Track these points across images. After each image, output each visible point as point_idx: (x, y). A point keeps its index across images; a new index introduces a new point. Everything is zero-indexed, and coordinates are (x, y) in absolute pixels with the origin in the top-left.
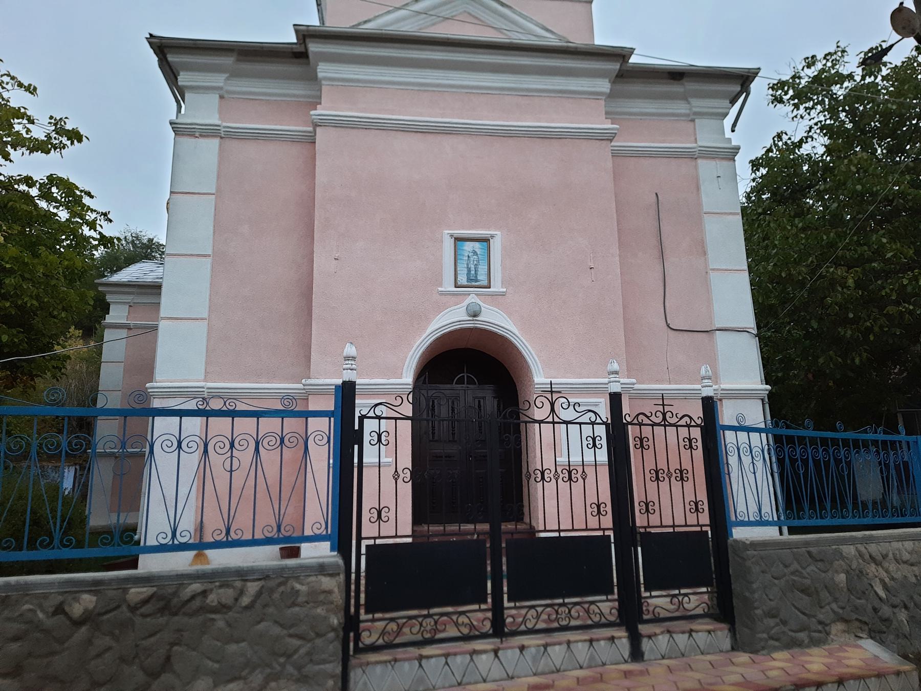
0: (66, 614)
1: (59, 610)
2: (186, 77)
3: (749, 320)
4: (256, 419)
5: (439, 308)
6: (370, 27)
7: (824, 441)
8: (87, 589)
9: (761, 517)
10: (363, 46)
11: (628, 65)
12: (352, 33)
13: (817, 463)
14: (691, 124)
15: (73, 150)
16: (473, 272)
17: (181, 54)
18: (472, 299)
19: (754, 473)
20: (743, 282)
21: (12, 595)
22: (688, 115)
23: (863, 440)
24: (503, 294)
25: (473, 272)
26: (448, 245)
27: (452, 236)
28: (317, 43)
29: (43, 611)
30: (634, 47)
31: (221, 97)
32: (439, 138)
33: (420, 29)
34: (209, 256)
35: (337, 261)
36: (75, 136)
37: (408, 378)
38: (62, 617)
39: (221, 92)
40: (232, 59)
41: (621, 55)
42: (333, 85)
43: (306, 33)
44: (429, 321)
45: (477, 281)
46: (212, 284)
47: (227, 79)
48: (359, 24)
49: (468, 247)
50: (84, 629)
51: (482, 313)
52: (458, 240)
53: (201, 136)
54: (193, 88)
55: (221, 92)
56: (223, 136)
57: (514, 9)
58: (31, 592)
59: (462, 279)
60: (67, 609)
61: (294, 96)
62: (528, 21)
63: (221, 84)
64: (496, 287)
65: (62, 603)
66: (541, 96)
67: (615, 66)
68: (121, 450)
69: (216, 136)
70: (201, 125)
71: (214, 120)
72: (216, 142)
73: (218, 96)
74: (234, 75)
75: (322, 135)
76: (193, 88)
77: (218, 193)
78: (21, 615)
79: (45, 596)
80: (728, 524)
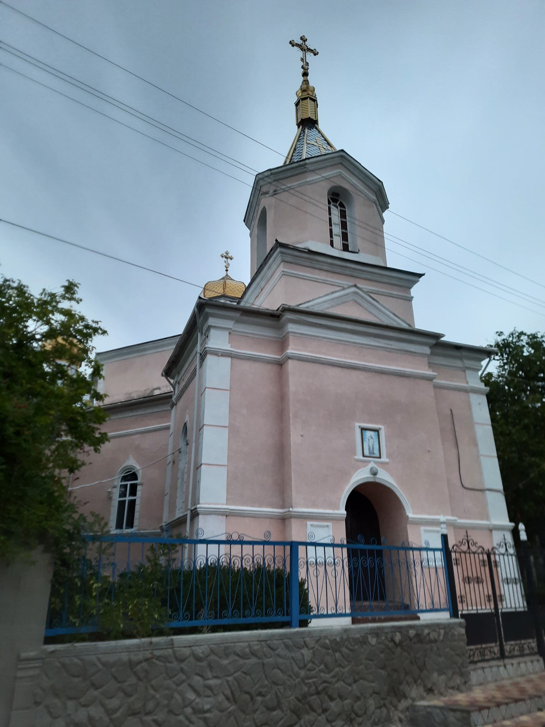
1: (392, 640)
3: (500, 486)
5: (356, 468)
7: (371, 552)
11: (439, 341)
13: (365, 569)
14: (463, 373)
18: (372, 465)
19: (317, 577)
20: (495, 462)
22: (462, 368)
23: (377, 551)
24: (387, 463)
26: (358, 432)
30: (444, 334)
31: (230, 333)
34: (227, 427)
35: (302, 437)
37: (343, 512)
39: (231, 331)
41: (437, 336)
45: (374, 454)
47: (234, 324)
49: (368, 434)
51: (378, 474)
52: (363, 429)
53: (222, 355)
54: (215, 327)
55: (231, 331)
64: (384, 459)
67: (433, 341)
70: (223, 350)
72: (229, 360)
74: (238, 321)
75: (291, 365)
76: (215, 327)
77: (231, 390)
79: (387, 633)
80: (451, 611)
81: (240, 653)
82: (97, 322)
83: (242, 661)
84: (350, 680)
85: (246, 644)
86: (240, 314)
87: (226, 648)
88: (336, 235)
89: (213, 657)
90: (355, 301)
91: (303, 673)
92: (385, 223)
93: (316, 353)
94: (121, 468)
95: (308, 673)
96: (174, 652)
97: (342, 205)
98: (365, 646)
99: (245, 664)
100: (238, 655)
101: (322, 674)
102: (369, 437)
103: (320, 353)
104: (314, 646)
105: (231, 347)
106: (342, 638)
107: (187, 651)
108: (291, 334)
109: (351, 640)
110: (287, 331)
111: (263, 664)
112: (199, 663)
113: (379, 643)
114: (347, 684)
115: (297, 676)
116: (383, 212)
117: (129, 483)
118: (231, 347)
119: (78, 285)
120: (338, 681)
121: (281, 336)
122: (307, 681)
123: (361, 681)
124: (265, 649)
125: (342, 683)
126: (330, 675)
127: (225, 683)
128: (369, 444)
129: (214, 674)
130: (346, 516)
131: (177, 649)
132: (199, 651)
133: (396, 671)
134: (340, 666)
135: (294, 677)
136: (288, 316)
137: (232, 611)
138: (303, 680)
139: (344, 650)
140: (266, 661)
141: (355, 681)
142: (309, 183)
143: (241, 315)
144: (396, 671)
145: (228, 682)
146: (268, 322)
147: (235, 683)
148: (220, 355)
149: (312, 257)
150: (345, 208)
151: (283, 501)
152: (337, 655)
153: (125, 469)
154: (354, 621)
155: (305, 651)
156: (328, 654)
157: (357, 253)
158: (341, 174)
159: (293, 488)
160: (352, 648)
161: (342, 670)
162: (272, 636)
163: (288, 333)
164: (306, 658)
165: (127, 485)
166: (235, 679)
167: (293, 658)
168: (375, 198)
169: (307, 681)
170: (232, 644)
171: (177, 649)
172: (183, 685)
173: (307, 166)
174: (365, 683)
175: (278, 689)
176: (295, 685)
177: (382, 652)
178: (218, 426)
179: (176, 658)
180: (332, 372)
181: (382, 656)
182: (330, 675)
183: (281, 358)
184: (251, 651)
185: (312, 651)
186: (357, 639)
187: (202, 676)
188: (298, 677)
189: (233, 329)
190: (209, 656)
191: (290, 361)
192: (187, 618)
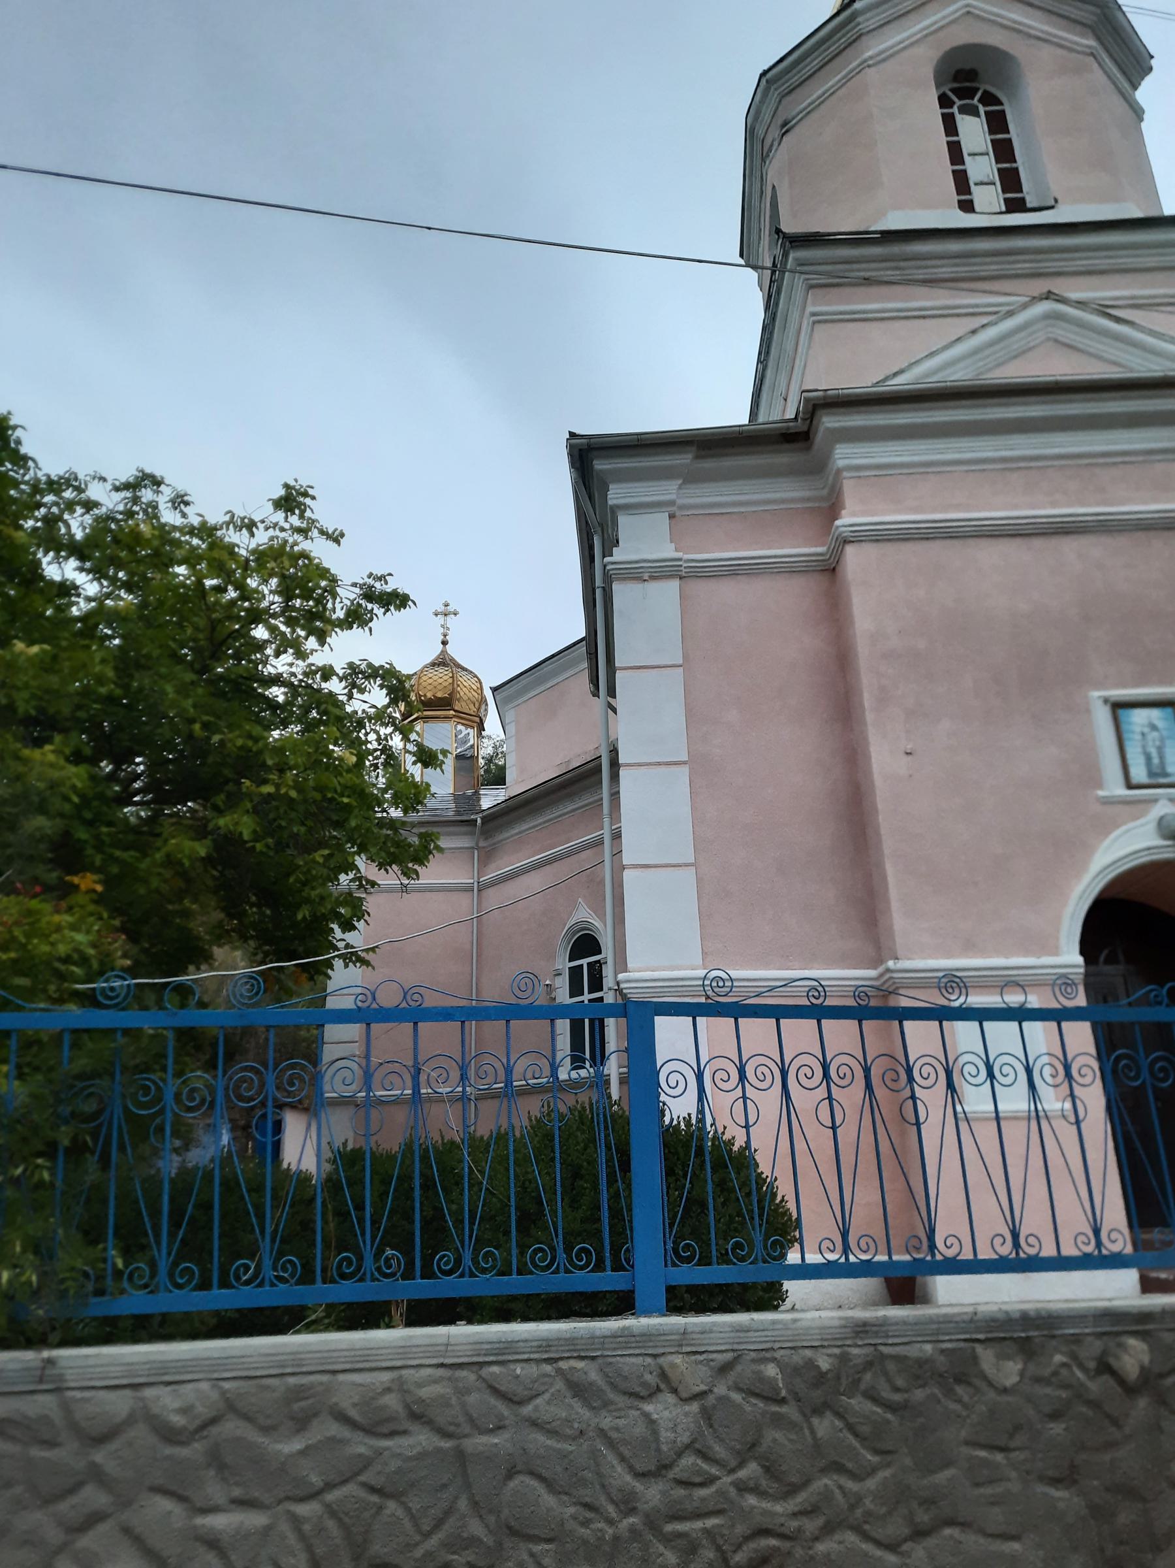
0: (1112, 1372)
1: (1105, 1367)
2: (619, 491)
4: (1015, 1024)
5: (1104, 827)
6: (902, 382)
8: (1134, 1328)
9: (1099, 1244)
10: (946, 408)
12: (875, 393)
15: (385, 621)
16: (1156, 761)
17: (612, 457)
21: (1035, 1337)
25: (1156, 761)
26: (1102, 717)
27: (1106, 701)
28: (834, 414)
29: (1081, 1366)
31: (672, 516)
32: (1054, 542)
33: (979, 374)
34: (684, 763)
35: (910, 757)
36: (396, 600)
37: (1071, 957)
38: (1106, 1378)
40: (690, 456)
42: (860, 477)
43: (816, 402)
44: (1088, 850)
45: (1166, 775)
46: (694, 809)
47: (680, 488)
48: (886, 379)
49: (1139, 717)
50: (1142, 1402)
52: (1118, 707)
53: (653, 578)
54: (627, 508)
56: (684, 575)
57: (1142, 326)
58: (1059, 1332)
59: (1139, 773)
60: (1112, 1361)
61: (783, 501)
62: (1166, 341)
63: (673, 497)
65: (1105, 1353)
66: (928, 473)
68: (460, 1089)
69: (671, 577)
71: (668, 551)
72: (675, 584)
73: (667, 514)
74: (690, 478)
75: (854, 559)
76: (627, 508)
77: (686, 663)
78: (1055, 1373)
79: (1077, 1339)
81: (353, 1413)
82: (381, 578)
83: (361, 1446)
84: (895, 1528)
85: (386, 1377)
86: (690, 456)
87: (298, 1393)
88: (982, 183)
89: (231, 1427)
90: (1056, 341)
91: (653, 1494)
92: (1145, 116)
93: (934, 510)
94: (566, 928)
95: (681, 1492)
96: (66, 1407)
97: (989, 99)
98: (960, 1390)
99: (379, 1453)
100: (342, 1418)
101: (752, 1500)
102: (1143, 726)
103: (945, 509)
104: (703, 1387)
105: (676, 550)
106: (844, 1359)
107: (120, 1404)
108: (845, 474)
109: (891, 1366)
110: (835, 468)
111: (460, 1456)
112: (169, 1451)
113: (1038, 1380)
114: (878, 1543)
115: (627, 1504)
116: (1135, 87)
117: (584, 962)
118: (676, 550)
119: (310, 491)
120: (828, 1529)
121: (825, 492)
122: (669, 1528)
123: (947, 1531)
124: (472, 1399)
125: (851, 1538)
126: (792, 1505)
127: (285, 1527)
128: (1144, 747)
129: (237, 1492)
130: (1082, 970)
131: (78, 1394)
132: (166, 1402)
133: (1130, 1492)
134: (837, 1467)
135: (611, 1509)
136: (829, 422)
137: (274, 1263)
138: (652, 1523)
139: (857, 1404)
140: (479, 1443)
141: (919, 1534)
142: (870, 62)
143: (697, 457)
144: (1130, 1492)
145: (296, 1521)
146: (783, 458)
147: (331, 1524)
148: (646, 576)
149: (896, 249)
150: (1001, 104)
151: (878, 946)
152: (824, 1426)
153: (572, 931)
154: (1148, 1285)
155: (663, 1409)
156: (777, 1420)
157: (1052, 207)
158: (971, 10)
159: (895, 905)
160: (897, 1397)
161: (850, 1485)
162: (504, 1352)
163: (839, 471)
164: (665, 1435)
165: (582, 965)
166: (331, 1511)
167: (602, 1433)
168: (1092, 42)
169: (669, 1528)
170: (325, 1378)
171: (78, 1394)
172: (103, 1528)
173: (860, 19)
174: (972, 1542)
175: (532, 1555)
176: (616, 1538)
177: (1055, 1416)
178: (659, 764)
179: (74, 1427)
180: (990, 554)
181: (1057, 1428)
182: (792, 1505)
183: (829, 548)
184: (407, 1406)
185: (695, 1407)
186: (921, 1362)
187: (181, 1499)
188: (632, 1511)
189: (680, 502)
190: (214, 1421)
191: (849, 550)
192: (189, 1281)
